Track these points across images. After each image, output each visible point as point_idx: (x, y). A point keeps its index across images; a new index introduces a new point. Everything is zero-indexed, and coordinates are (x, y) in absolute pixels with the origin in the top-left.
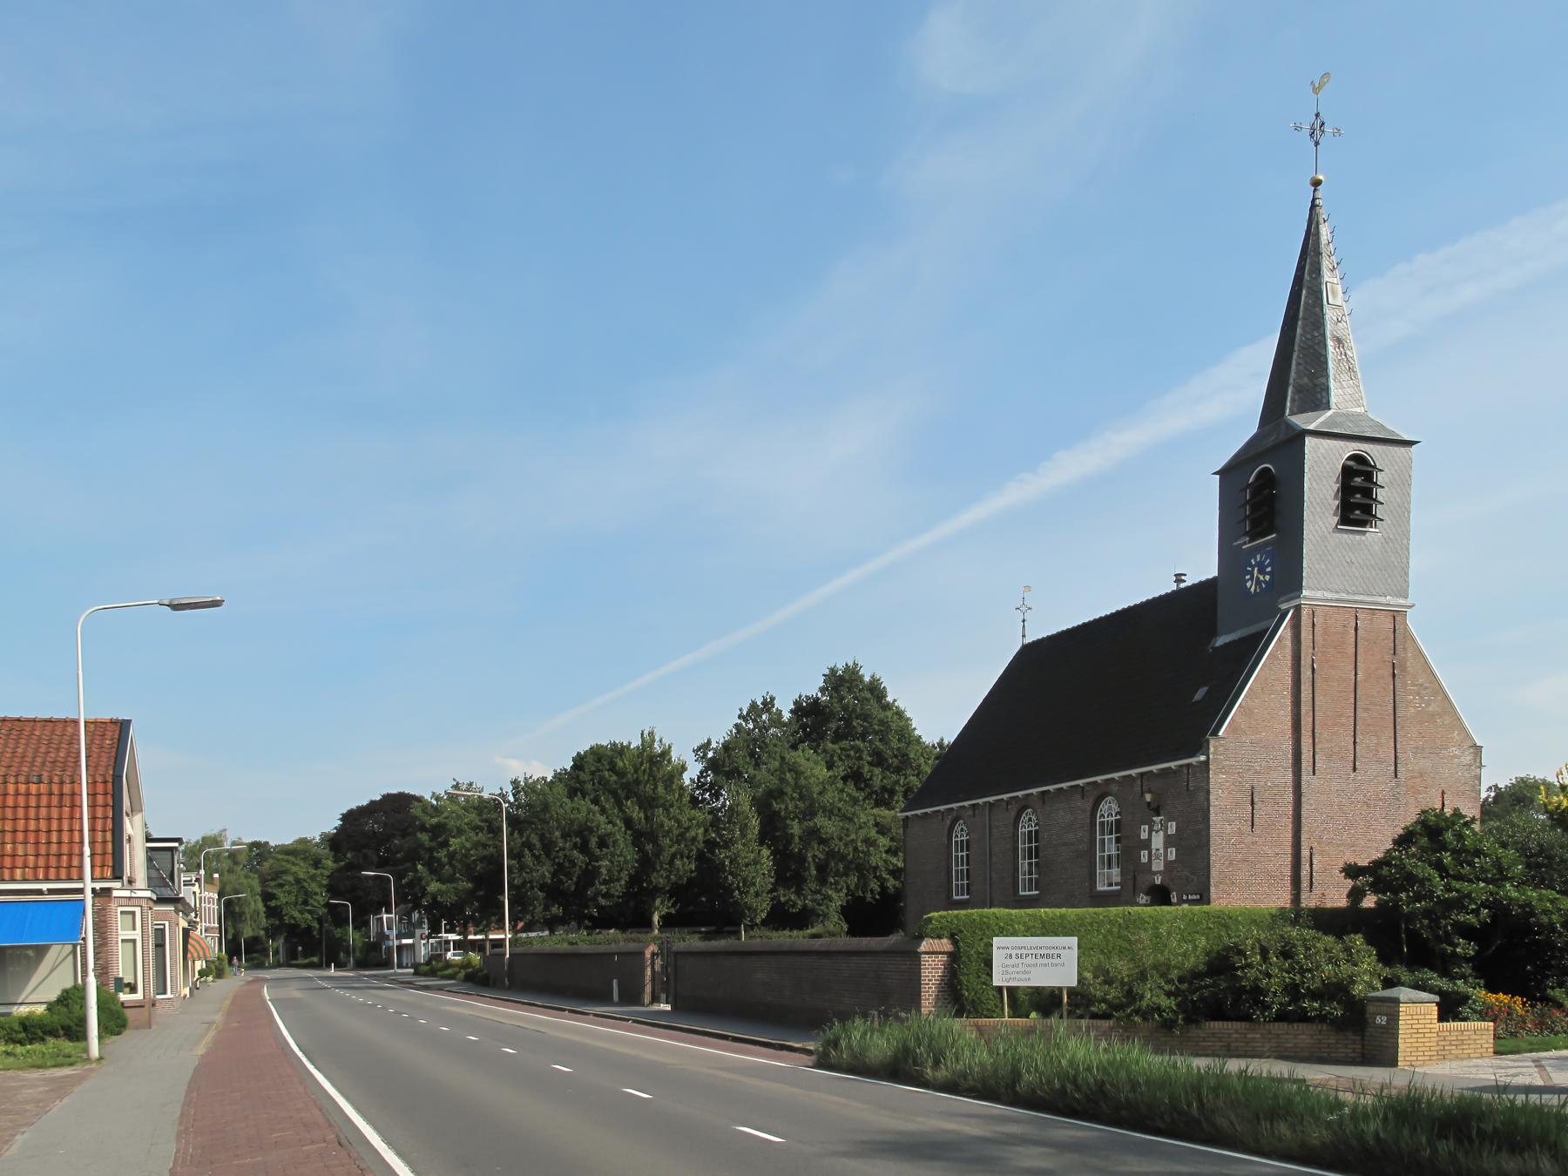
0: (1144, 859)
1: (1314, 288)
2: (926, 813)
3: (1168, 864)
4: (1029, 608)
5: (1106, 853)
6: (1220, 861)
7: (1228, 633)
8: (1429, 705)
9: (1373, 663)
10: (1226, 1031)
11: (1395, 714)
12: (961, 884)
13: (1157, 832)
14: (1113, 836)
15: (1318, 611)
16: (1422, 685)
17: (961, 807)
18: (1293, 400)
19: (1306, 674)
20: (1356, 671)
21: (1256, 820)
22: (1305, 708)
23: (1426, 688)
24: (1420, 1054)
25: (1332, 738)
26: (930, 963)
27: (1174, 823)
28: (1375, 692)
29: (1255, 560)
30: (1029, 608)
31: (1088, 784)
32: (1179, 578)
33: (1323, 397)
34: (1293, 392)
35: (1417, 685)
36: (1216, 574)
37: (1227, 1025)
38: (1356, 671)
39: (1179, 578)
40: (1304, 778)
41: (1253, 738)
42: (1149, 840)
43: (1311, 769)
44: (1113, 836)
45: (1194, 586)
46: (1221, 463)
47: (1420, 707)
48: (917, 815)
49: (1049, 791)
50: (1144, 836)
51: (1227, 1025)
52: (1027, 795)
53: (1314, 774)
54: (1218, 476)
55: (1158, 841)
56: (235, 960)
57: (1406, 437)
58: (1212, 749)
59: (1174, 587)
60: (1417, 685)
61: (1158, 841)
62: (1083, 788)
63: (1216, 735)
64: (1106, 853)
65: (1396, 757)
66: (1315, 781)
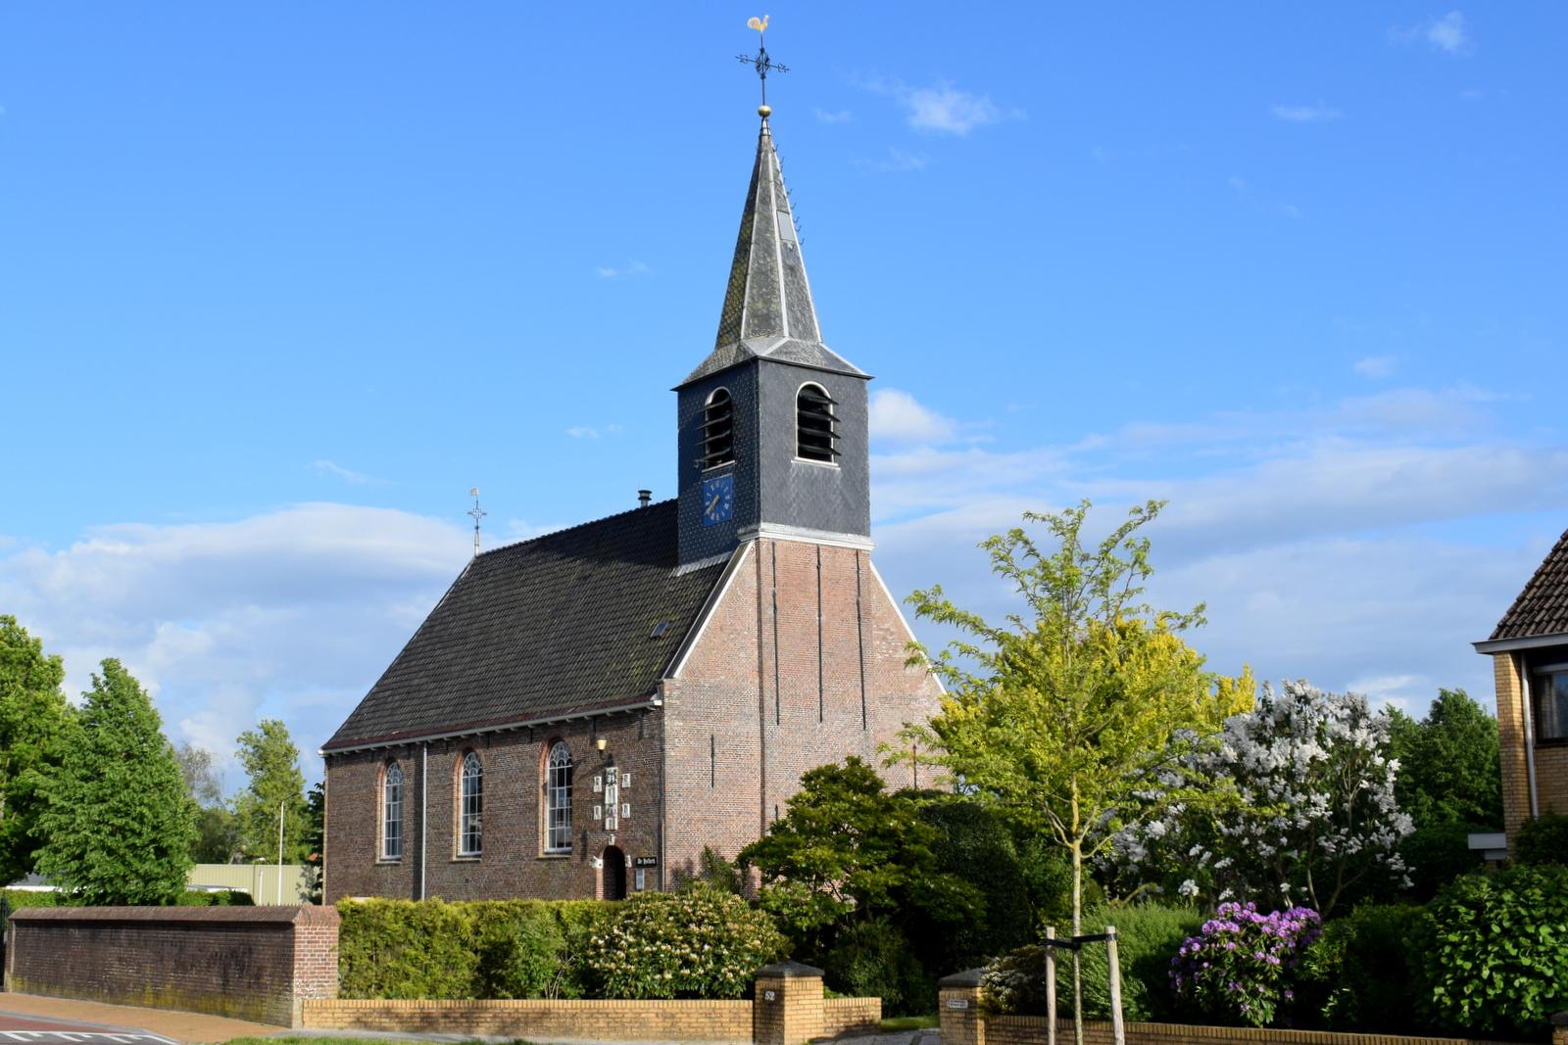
0: (598, 816)
1: (766, 214)
2: (353, 752)
3: (623, 822)
4: (470, 513)
5: (557, 807)
6: (677, 819)
7: (689, 562)
8: (897, 651)
9: (839, 599)
10: (620, 1011)
11: (861, 660)
12: (393, 840)
13: (612, 784)
14: (565, 787)
15: (777, 543)
16: (888, 630)
17: (394, 746)
18: (748, 324)
19: (768, 612)
20: (820, 611)
21: (716, 775)
22: (769, 649)
23: (892, 634)
24: (806, 1031)
25: (800, 682)
26: (313, 949)
27: (629, 775)
28: (840, 631)
29: (714, 486)
30: (470, 513)
31: (538, 725)
32: (645, 495)
33: (776, 324)
34: (747, 316)
35: (881, 630)
36: (675, 496)
37: (730, 1004)
38: (820, 611)
39: (645, 495)
40: (768, 728)
41: (712, 681)
42: (603, 793)
43: (774, 718)
44: (565, 787)
45: (658, 505)
46: (680, 382)
47: (888, 653)
48: (342, 753)
49: (494, 732)
50: (597, 788)
51: (730, 1004)
52: (470, 735)
53: (778, 724)
54: (676, 393)
55: (612, 796)
56: (810, 471)
57: (863, 373)
58: (667, 693)
59: (638, 505)
60: (881, 630)
61: (612, 796)
62: (531, 730)
63: (672, 678)
64: (557, 807)
65: (864, 708)
66: (780, 732)
